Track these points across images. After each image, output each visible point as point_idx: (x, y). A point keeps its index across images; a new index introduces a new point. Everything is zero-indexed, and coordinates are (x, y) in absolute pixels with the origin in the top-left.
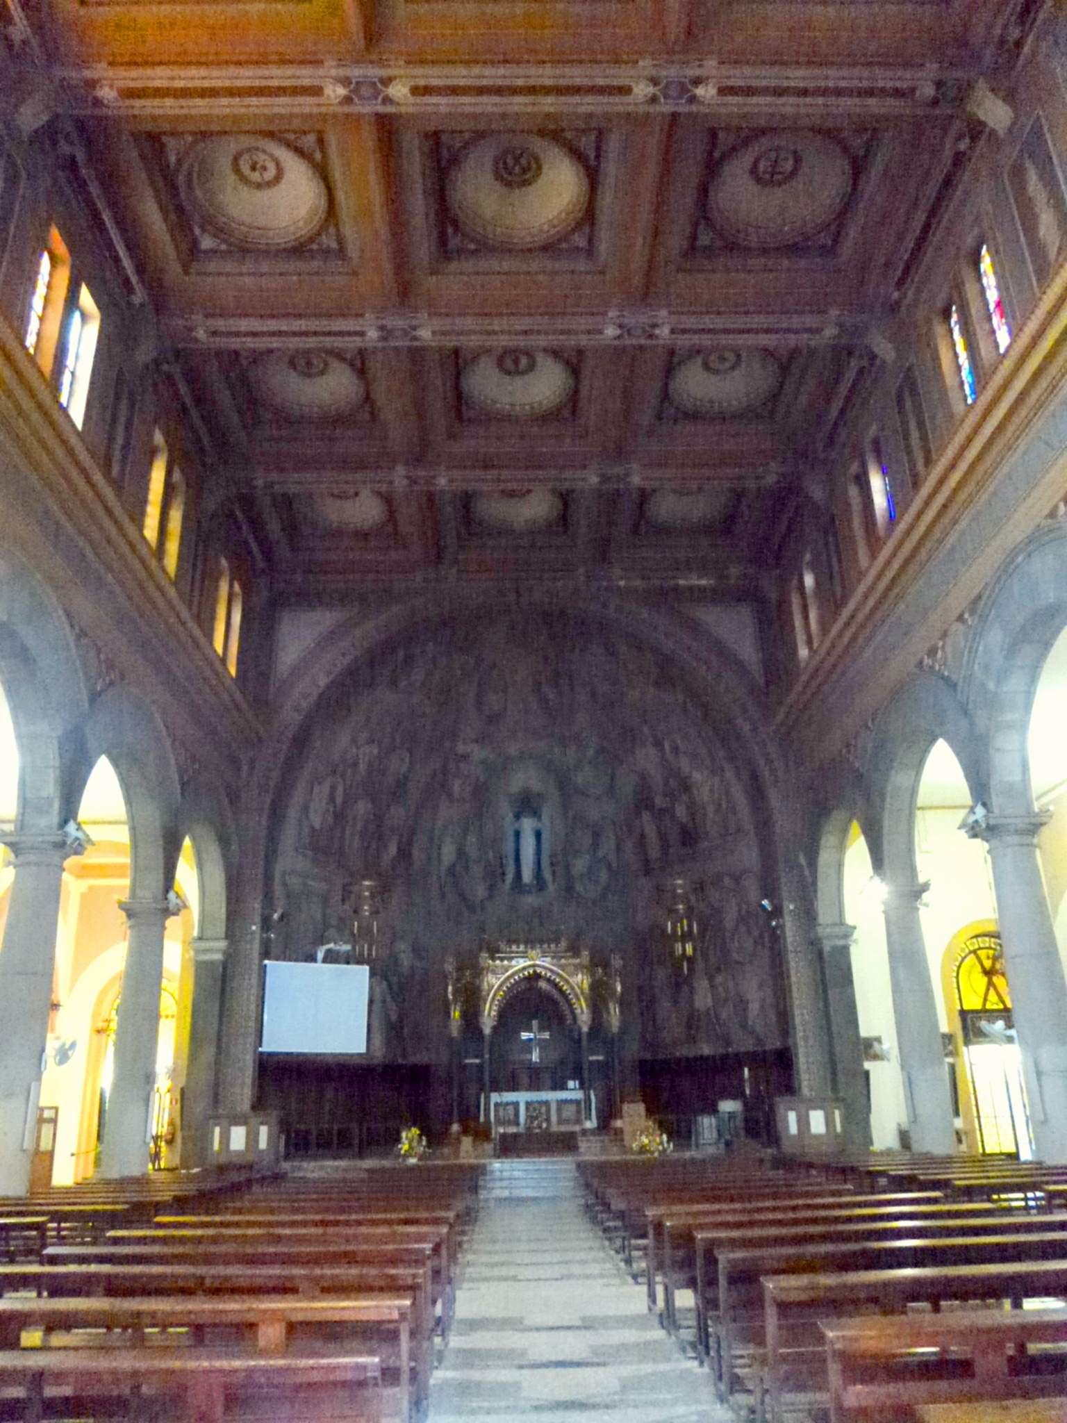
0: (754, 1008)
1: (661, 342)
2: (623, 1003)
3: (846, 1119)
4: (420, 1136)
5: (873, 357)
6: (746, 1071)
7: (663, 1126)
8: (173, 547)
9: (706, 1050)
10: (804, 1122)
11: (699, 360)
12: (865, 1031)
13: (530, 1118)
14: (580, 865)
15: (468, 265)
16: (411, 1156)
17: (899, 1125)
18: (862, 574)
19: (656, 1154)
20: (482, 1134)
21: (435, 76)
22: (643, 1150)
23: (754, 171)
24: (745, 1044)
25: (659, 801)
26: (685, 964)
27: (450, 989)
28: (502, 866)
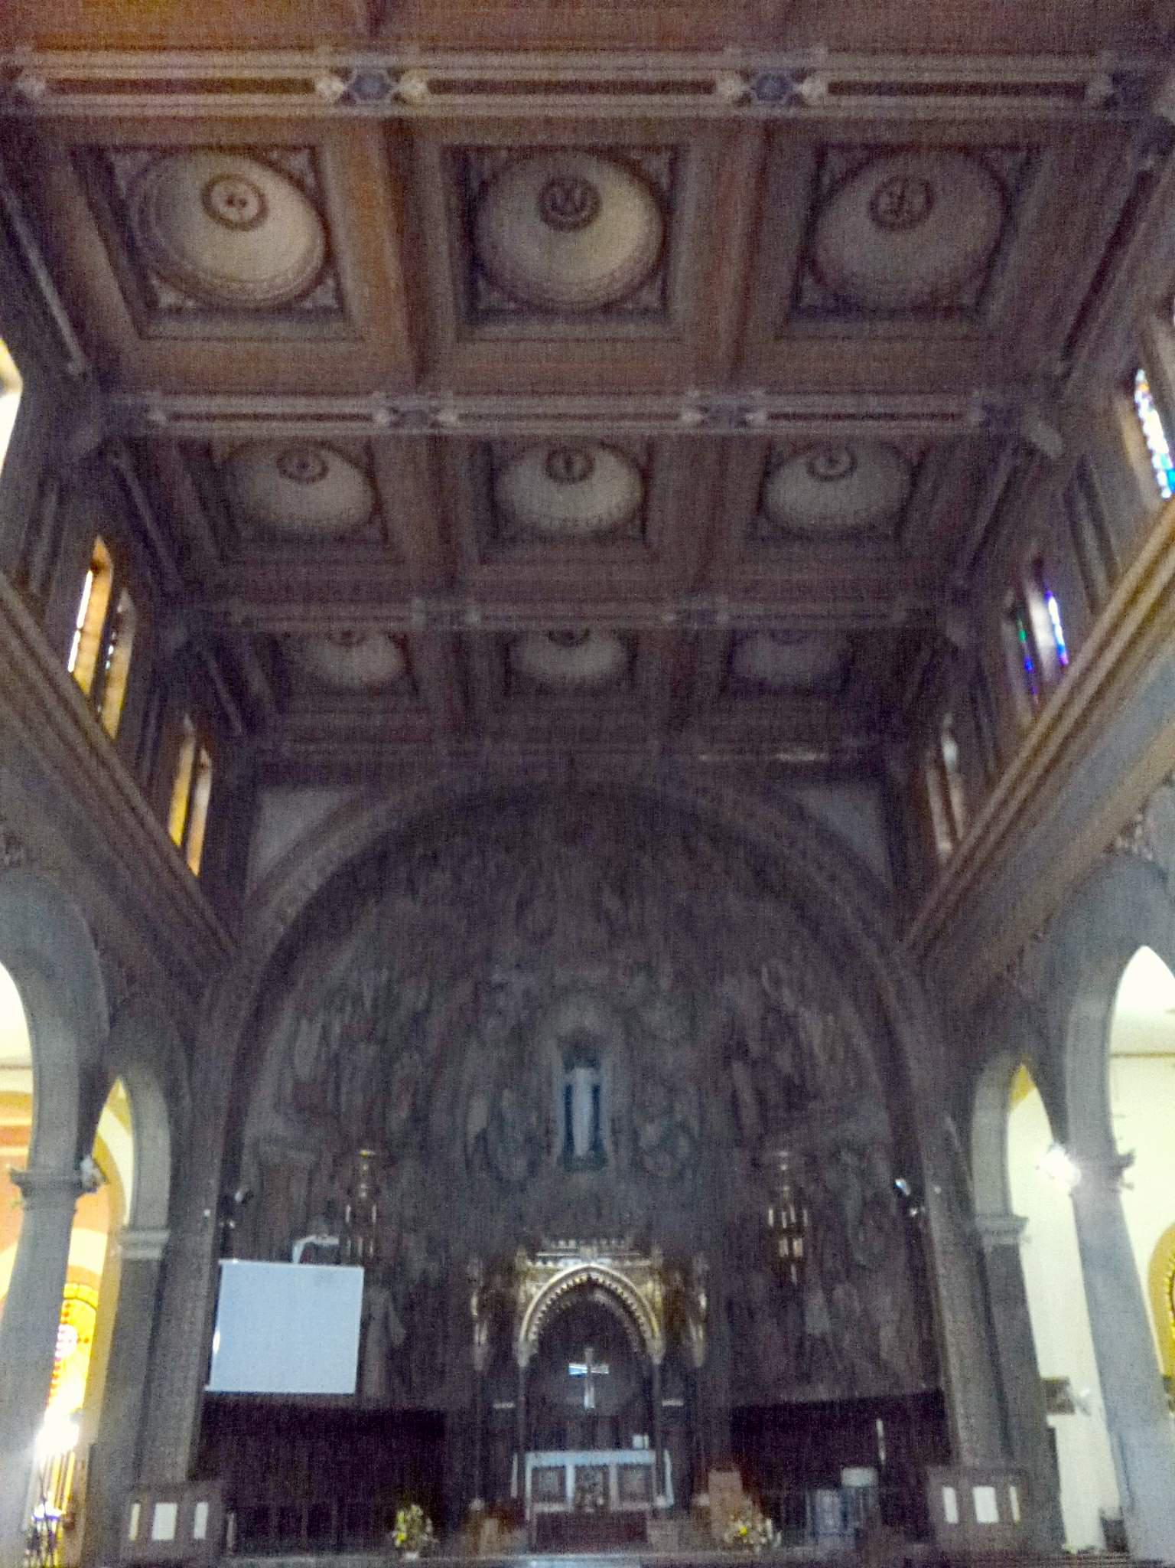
0: (887, 1334)
1: (756, 432)
2: (707, 1322)
3: (1026, 1499)
4: (423, 1518)
5: (1031, 452)
6: (879, 1425)
7: (769, 1508)
8: (116, 695)
9: (822, 1393)
10: (966, 1506)
11: (801, 460)
12: (1048, 1368)
13: (580, 1489)
14: (651, 1133)
15: (508, 330)
16: (410, 1549)
17: (1102, 1512)
18: (1023, 736)
19: (758, 1549)
20: (511, 1516)
21: (463, 67)
22: (739, 1542)
23: (873, 206)
24: (872, 1387)
25: (755, 1049)
26: (793, 1269)
27: (474, 1301)
28: (548, 1132)
